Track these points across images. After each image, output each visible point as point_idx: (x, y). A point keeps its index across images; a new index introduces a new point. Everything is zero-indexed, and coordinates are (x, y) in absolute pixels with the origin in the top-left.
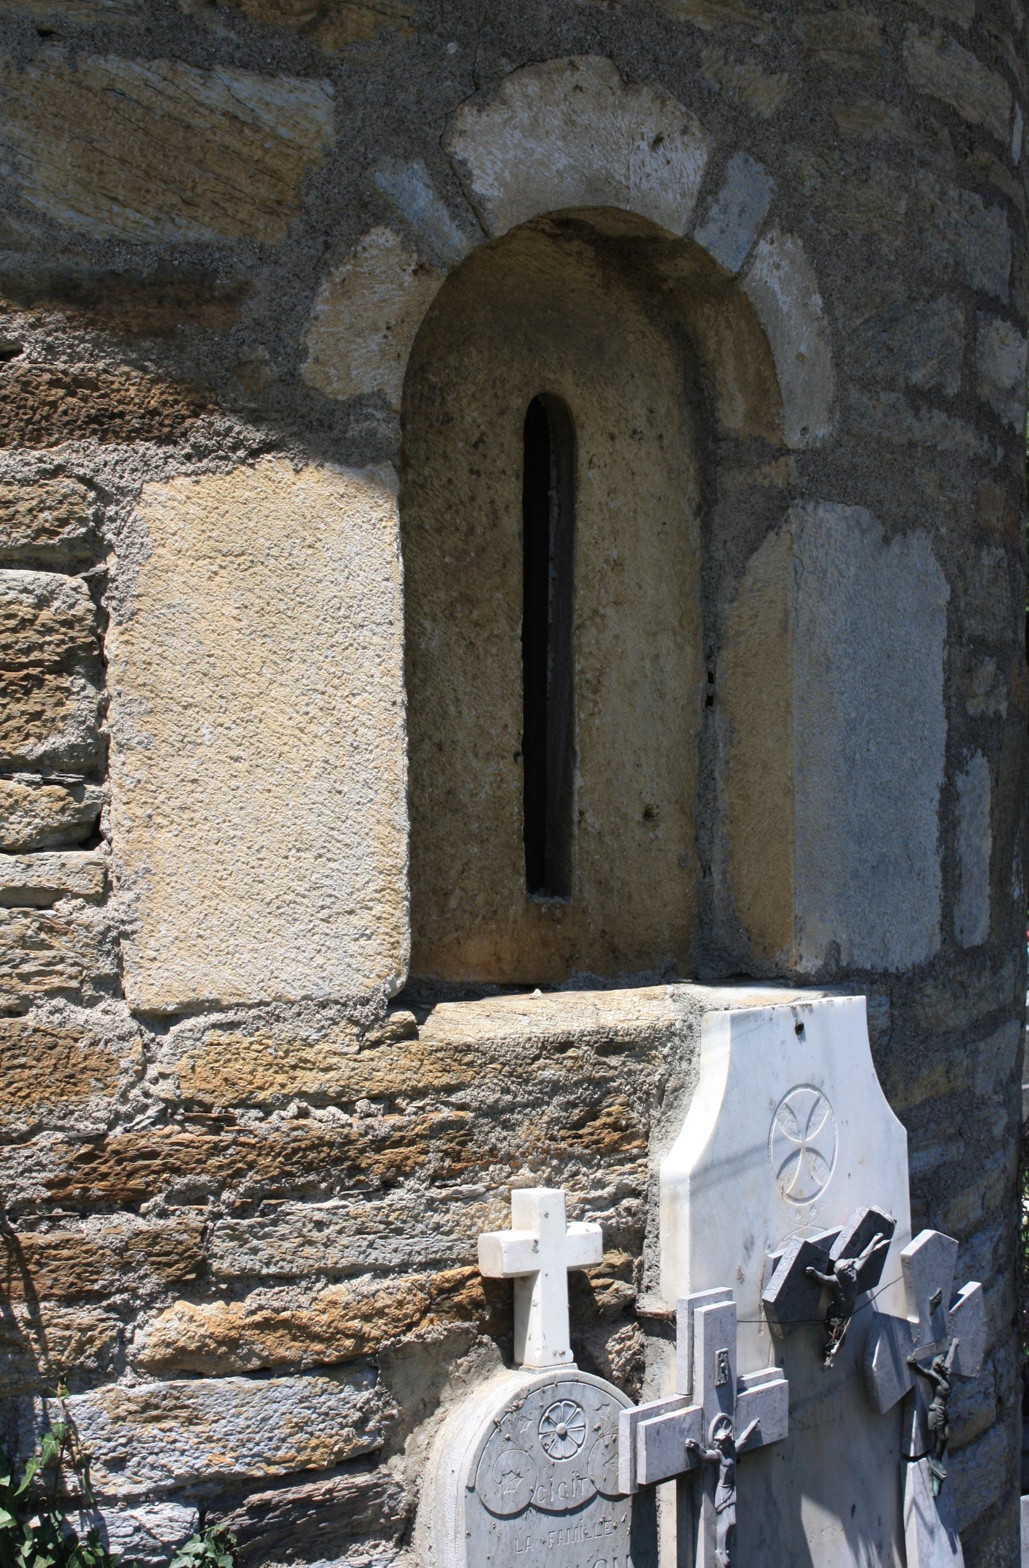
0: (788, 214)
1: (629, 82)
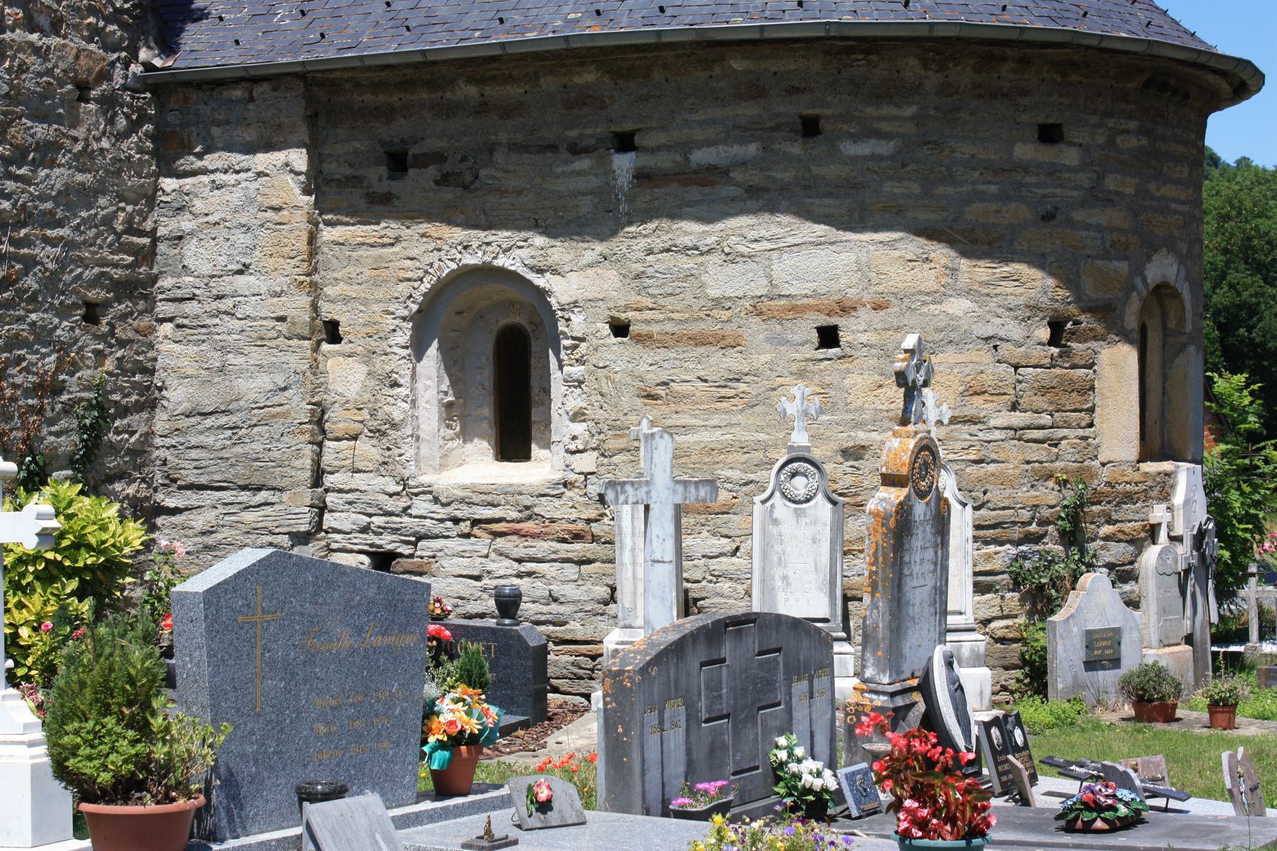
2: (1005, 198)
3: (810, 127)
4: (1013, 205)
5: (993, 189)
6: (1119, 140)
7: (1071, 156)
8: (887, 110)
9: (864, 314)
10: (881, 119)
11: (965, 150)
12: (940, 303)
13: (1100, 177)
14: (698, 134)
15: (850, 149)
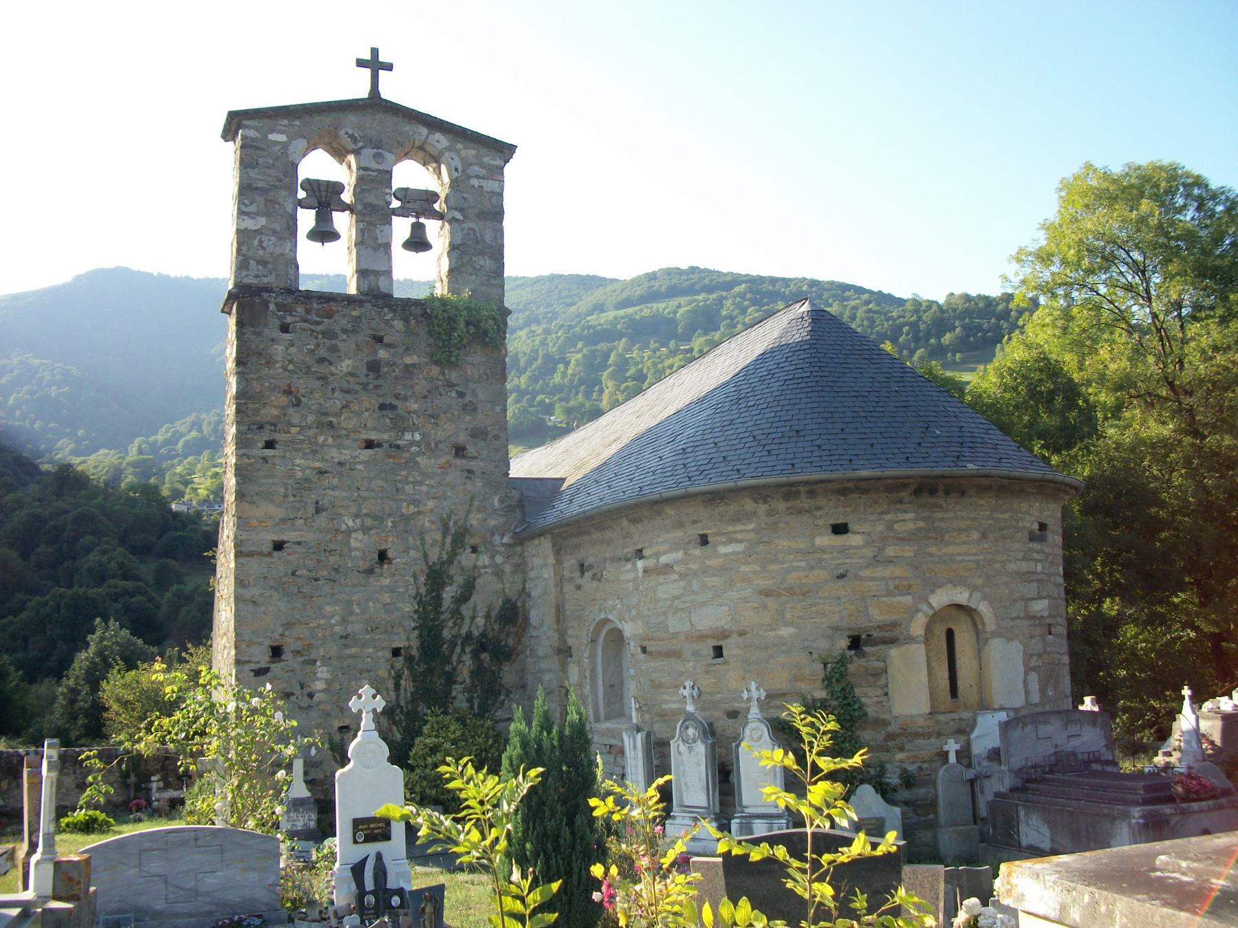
0: (985, 597)
1: (955, 586)
2: (812, 568)
3: (704, 540)
4: (816, 572)
5: (803, 564)
6: (896, 526)
7: (853, 540)
8: (739, 527)
9: (734, 638)
10: (735, 532)
11: (783, 544)
12: (775, 629)
13: (881, 550)
14: (662, 548)
15: (723, 550)
